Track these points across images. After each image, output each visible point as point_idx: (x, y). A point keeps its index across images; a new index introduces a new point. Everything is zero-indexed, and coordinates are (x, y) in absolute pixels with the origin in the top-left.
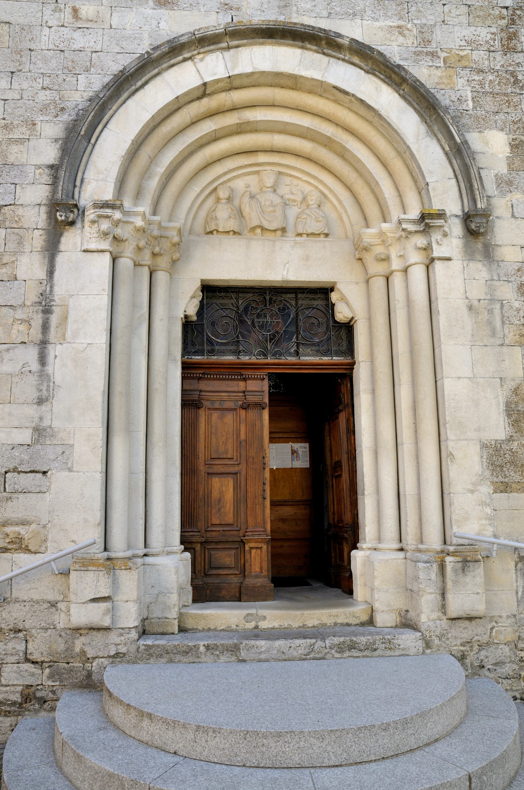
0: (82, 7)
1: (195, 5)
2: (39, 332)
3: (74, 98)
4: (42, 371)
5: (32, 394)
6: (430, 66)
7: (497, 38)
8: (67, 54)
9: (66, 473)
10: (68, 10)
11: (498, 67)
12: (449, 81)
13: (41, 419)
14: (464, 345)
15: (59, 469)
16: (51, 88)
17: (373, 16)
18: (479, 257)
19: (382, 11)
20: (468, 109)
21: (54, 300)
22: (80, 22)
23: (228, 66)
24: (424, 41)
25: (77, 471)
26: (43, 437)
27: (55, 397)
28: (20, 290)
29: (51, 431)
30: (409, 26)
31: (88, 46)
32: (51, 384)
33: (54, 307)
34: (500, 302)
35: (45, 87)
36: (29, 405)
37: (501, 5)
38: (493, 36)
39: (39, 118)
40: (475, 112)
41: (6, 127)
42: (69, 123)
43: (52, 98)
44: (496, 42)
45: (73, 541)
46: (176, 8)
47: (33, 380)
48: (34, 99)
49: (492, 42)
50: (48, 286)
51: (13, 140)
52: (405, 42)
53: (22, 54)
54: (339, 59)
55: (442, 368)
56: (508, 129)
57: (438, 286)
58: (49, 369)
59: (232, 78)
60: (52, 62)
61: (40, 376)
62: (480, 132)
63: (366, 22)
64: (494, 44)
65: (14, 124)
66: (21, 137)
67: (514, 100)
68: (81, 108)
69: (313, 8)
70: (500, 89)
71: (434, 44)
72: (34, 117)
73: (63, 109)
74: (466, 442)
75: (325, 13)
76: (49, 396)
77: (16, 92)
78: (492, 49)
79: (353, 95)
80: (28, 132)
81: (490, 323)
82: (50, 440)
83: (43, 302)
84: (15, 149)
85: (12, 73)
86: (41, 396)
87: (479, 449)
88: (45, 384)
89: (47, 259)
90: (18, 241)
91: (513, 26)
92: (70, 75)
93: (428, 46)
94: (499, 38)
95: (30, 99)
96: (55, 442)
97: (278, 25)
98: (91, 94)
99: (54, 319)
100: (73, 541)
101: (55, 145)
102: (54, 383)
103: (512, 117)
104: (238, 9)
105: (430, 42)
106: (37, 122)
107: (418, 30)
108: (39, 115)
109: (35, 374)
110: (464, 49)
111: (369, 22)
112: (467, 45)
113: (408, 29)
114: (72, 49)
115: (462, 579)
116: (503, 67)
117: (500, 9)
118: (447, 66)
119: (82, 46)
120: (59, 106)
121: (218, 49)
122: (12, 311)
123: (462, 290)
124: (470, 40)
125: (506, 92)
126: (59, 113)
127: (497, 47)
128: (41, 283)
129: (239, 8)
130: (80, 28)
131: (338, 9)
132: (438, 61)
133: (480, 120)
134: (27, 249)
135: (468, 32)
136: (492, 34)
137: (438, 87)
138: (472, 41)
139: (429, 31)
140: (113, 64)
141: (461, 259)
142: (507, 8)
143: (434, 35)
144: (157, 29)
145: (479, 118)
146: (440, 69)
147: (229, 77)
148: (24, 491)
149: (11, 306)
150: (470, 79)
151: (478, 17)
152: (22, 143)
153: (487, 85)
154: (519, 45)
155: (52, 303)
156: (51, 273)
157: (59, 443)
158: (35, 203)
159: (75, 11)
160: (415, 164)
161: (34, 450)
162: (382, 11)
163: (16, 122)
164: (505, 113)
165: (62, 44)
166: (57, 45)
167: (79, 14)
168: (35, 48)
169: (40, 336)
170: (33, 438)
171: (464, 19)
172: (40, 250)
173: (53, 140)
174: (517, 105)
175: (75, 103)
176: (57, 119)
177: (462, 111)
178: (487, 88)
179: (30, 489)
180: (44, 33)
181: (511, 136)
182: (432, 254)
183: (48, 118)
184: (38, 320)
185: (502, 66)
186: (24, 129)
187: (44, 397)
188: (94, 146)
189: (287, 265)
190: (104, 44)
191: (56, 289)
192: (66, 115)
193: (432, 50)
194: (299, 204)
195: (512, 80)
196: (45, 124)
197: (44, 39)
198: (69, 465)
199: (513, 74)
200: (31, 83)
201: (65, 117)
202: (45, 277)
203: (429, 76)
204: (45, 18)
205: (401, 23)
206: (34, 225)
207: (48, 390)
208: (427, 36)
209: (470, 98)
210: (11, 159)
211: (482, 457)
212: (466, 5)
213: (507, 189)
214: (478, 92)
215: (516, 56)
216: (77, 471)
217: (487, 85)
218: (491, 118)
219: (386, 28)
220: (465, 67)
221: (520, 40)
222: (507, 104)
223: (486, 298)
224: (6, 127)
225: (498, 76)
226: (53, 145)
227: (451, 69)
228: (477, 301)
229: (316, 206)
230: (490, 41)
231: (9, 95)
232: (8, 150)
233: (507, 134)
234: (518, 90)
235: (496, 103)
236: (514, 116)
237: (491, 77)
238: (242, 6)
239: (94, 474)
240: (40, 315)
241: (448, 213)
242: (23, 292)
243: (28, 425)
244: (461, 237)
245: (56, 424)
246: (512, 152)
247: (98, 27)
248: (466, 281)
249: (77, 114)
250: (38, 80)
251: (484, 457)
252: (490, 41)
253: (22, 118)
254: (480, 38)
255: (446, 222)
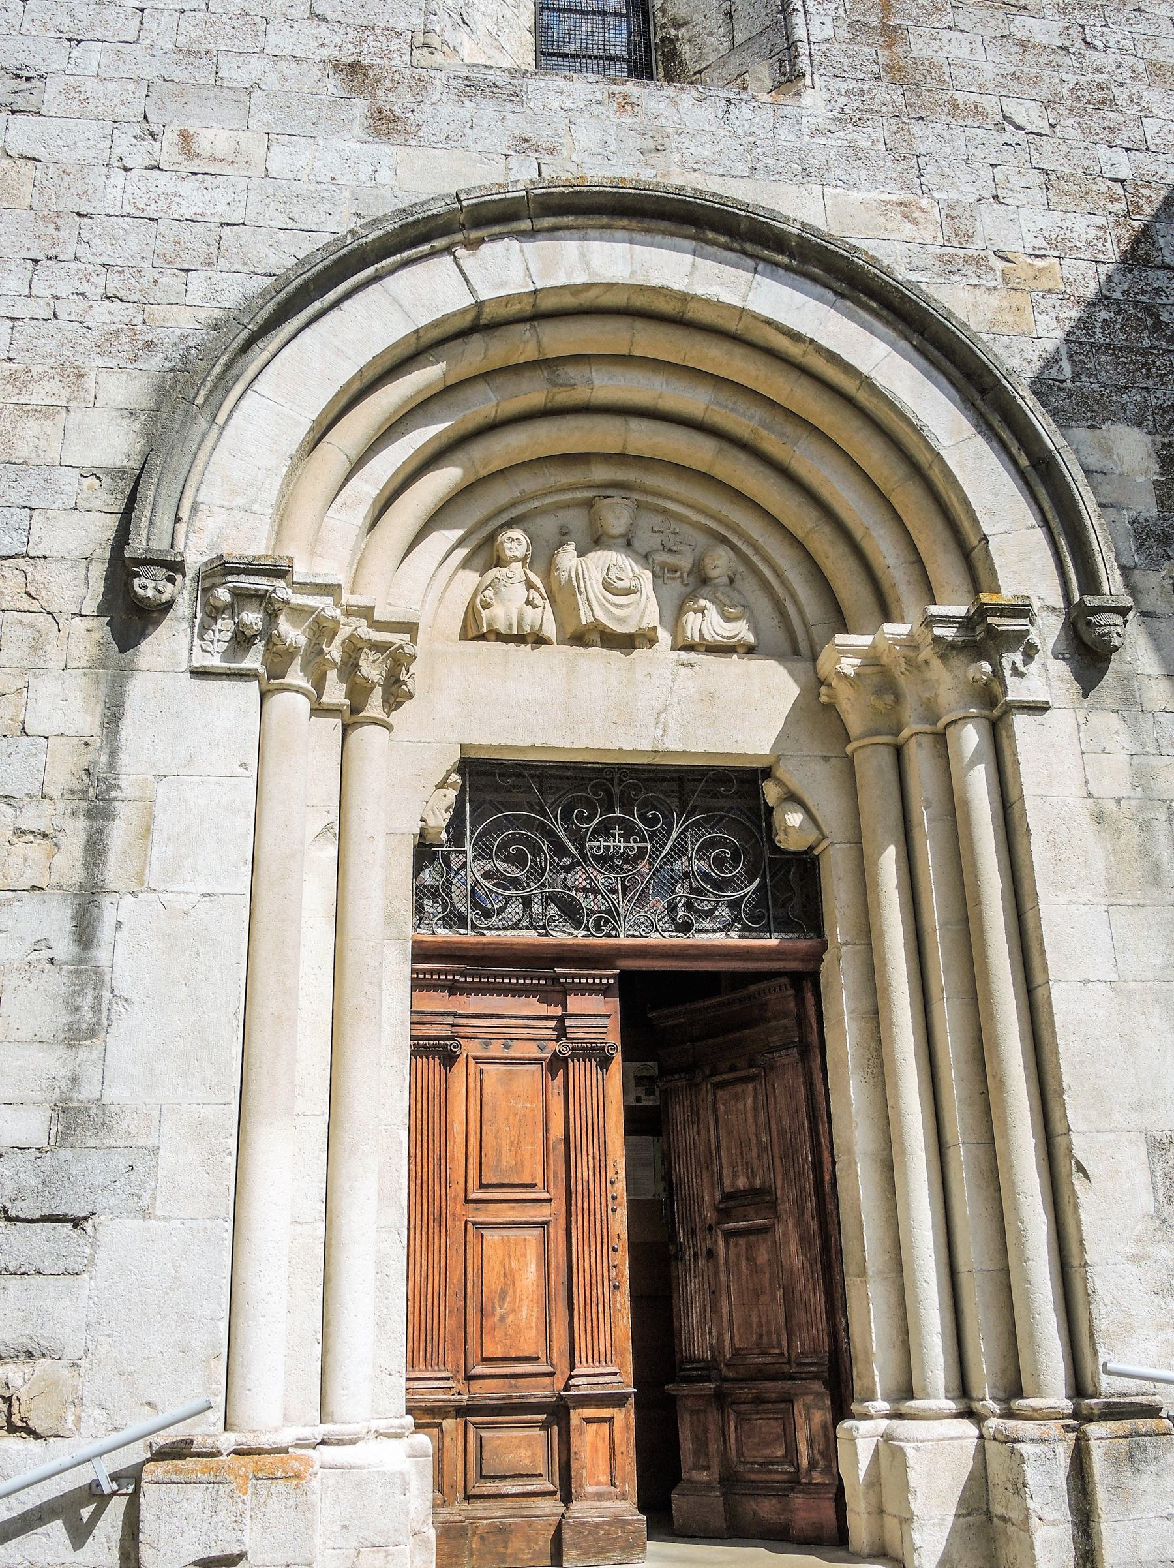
0: (203, 132)
1: (456, 138)
2: (79, 864)
3: (177, 321)
4: (80, 961)
5: (54, 1017)
6: (976, 286)
7: (1108, 236)
8: (162, 226)
9: (137, 1222)
10: (170, 138)
11: (1117, 295)
12: (1017, 319)
13: (75, 1080)
14: (1089, 903)
15: (117, 1212)
16: (124, 298)
17: (844, 178)
18: (1110, 702)
19: (863, 172)
20: (1062, 377)
21: (116, 787)
22: (196, 161)
23: (531, 269)
24: (957, 235)
25: (163, 1218)
26: (79, 1129)
27: (114, 1025)
28: (32, 760)
29: (101, 1114)
30: (924, 202)
31: (214, 211)
32: (106, 994)
33: (116, 804)
34: (1166, 805)
35: (109, 295)
36: (45, 1046)
37: (1109, 176)
38: (1100, 233)
39: (92, 362)
40: (1078, 384)
41: (12, 378)
42: (163, 377)
43: (127, 321)
44: (1109, 245)
45: (149, 1404)
46: (413, 142)
47: (56, 982)
48: (82, 319)
49: (1100, 245)
50: (105, 751)
51: (29, 408)
52: (918, 236)
53: (59, 223)
54: (777, 264)
55: (1044, 959)
56: (1150, 423)
57: (1023, 769)
58: (101, 955)
59: (539, 295)
60: (129, 242)
61: (78, 973)
62: (1093, 427)
63: (831, 190)
64: (1103, 248)
65: (34, 372)
66: (48, 401)
67: (1158, 364)
68: (193, 344)
69: (716, 157)
70: (1126, 340)
71: (979, 242)
72: (81, 358)
73: (149, 344)
74: (1112, 1136)
75: (742, 168)
76: (98, 1022)
77: (42, 302)
78: (1101, 257)
79: (812, 341)
80: (66, 392)
81: (1145, 852)
82: (97, 1136)
83: (91, 789)
84: (31, 427)
85: (36, 261)
86: (78, 1022)
87: (1144, 1155)
88: (90, 994)
89: (102, 687)
90: (33, 643)
91: (1138, 217)
92: (169, 271)
93: (967, 246)
94: (1114, 237)
95: (73, 319)
96: (109, 1142)
97: (645, 189)
98: (217, 314)
99: (119, 834)
100: (149, 1404)
101: (129, 425)
102: (112, 991)
103: (1158, 398)
104: (552, 151)
105: (970, 237)
106: (87, 370)
107: (943, 212)
108: (94, 355)
109: (65, 967)
110: (1045, 256)
111: (839, 190)
112: (1048, 247)
113: (922, 210)
114: (176, 217)
115: (1131, 1481)
116: (1128, 295)
117: (1108, 183)
118: (1010, 286)
119: (199, 211)
120: (140, 337)
121: (510, 234)
122: (10, 810)
123: (1078, 777)
124: (1053, 237)
125: (1140, 345)
126: (141, 353)
127: (1111, 255)
128: (86, 744)
129: (555, 148)
130: (196, 174)
131: (770, 162)
132: (990, 276)
133: (1090, 402)
134: (55, 659)
135: (1048, 221)
136: (1099, 228)
137: (994, 330)
138: (1059, 239)
139: (968, 215)
140: (269, 252)
141: (1071, 705)
142: (1122, 181)
143: (978, 224)
144: (372, 184)
145: (1087, 398)
146: (996, 293)
147: (535, 292)
148: (22, 1270)
149: (7, 797)
150: (1062, 316)
151: (1067, 194)
152: (51, 417)
153: (1098, 330)
154: (1155, 254)
155: (113, 794)
156: (113, 716)
157: (121, 1143)
158: (77, 554)
159: (186, 138)
160: (955, 494)
161: (55, 1162)
162: (863, 172)
163: (36, 369)
164: (1142, 388)
165: (153, 206)
166: (140, 207)
167: (195, 146)
168: (90, 211)
169: (79, 874)
170: (53, 1132)
171: (1038, 195)
172: (84, 663)
173: (126, 413)
174: (1165, 374)
175: (179, 331)
176: (136, 365)
177: (1051, 382)
178: (1098, 335)
179: (41, 1267)
180: (113, 181)
181: (1159, 438)
182: (1005, 694)
183: (114, 363)
184: (76, 832)
185: (1125, 292)
186: (55, 385)
187: (84, 1027)
188: (222, 429)
189: (664, 715)
190: (249, 207)
191: (125, 761)
192: (157, 359)
193: (975, 254)
194: (685, 575)
195: (1150, 322)
196: (105, 375)
197: (113, 193)
198: (146, 1201)
199: (1150, 310)
200: (77, 284)
201: (155, 362)
202: (96, 730)
203: (975, 306)
204: (117, 151)
205: (906, 196)
206: (74, 605)
207: (96, 1008)
208: (964, 225)
209: (1065, 356)
210: (23, 451)
211: (1153, 1173)
212: (1039, 169)
213: (1161, 552)
214: (1082, 343)
215: (1152, 274)
216: (163, 1218)
217: (1098, 330)
218: (1114, 398)
219: (875, 204)
220: (1050, 291)
221: (1157, 245)
222: (1144, 371)
223: (1133, 795)
224: (12, 378)
225: (1119, 313)
226: (124, 423)
227: (1019, 293)
228: (1113, 802)
229: (725, 580)
230: (1095, 242)
231: (23, 309)
232: (17, 431)
233: (1149, 433)
234: (1164, 344)
235: (1120, 367)
236: (1159, 397)
237: (1104, 315)
238: (562, 144)
239: (209, 1223)
240: (81, 823)
241: (1036, 605)
242: (41, 766)
243: (39, 1096)
244: (1067, 656)
245: (114, 1095)
246: (1164, 471)
247: (237, 173)
248: (1085, 756)
249: (184, 358)
250: (94, 278)
251: (1158, 1174)
252: (1095, 242)
253: (53, 360)
254: (1075, 235)
255: (1032, 623)
